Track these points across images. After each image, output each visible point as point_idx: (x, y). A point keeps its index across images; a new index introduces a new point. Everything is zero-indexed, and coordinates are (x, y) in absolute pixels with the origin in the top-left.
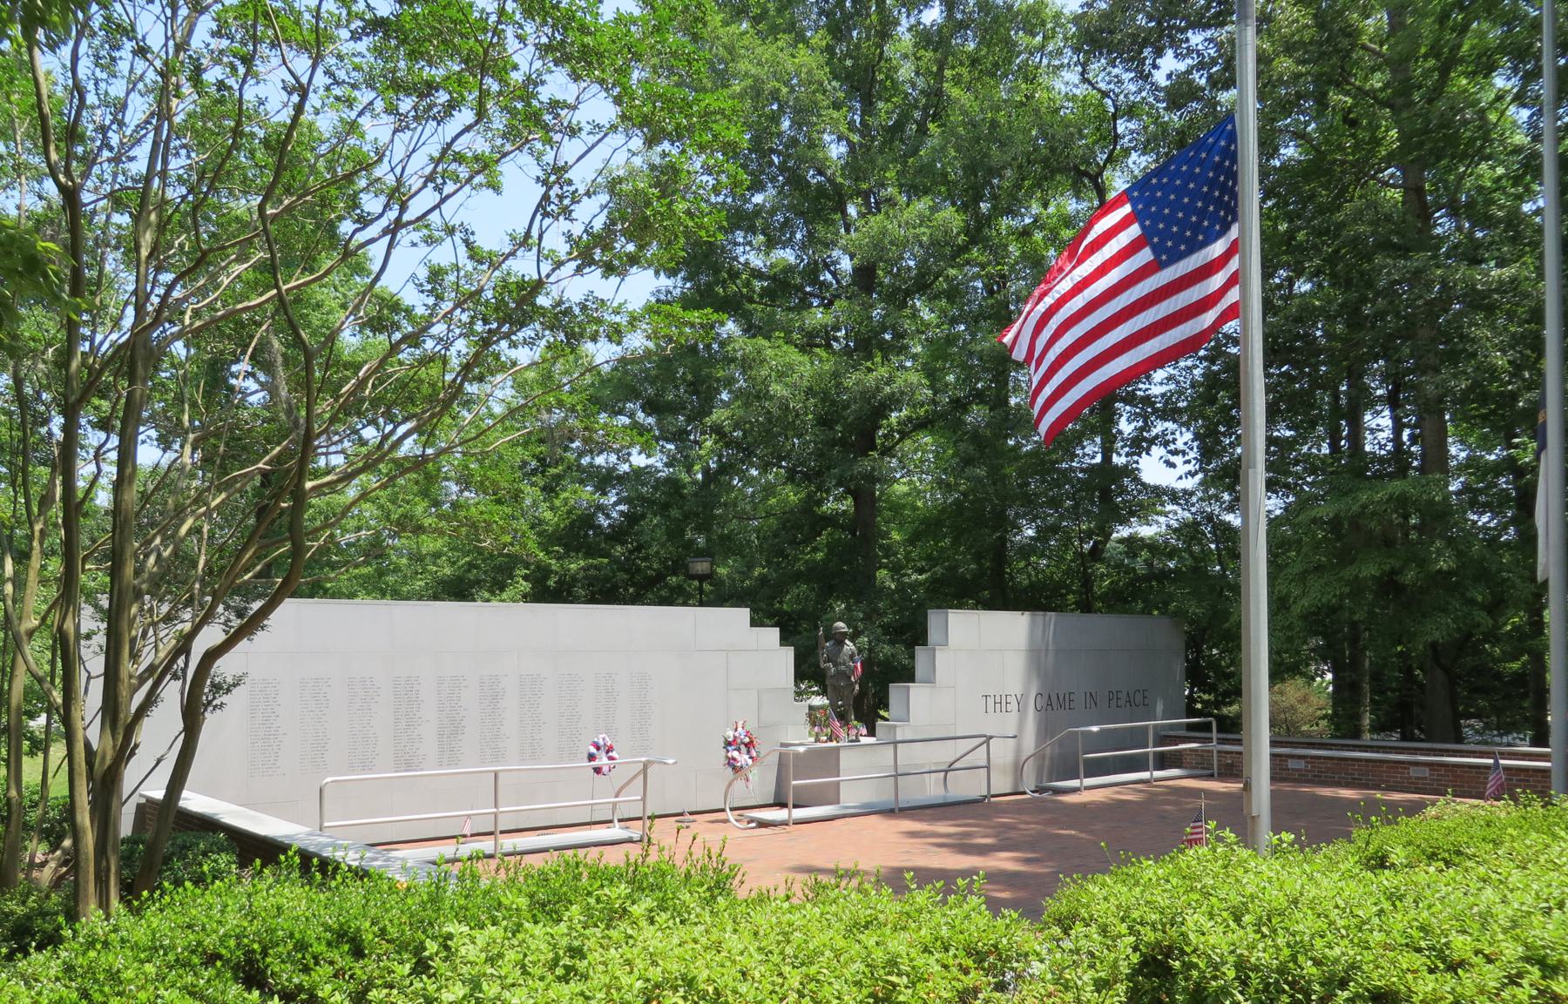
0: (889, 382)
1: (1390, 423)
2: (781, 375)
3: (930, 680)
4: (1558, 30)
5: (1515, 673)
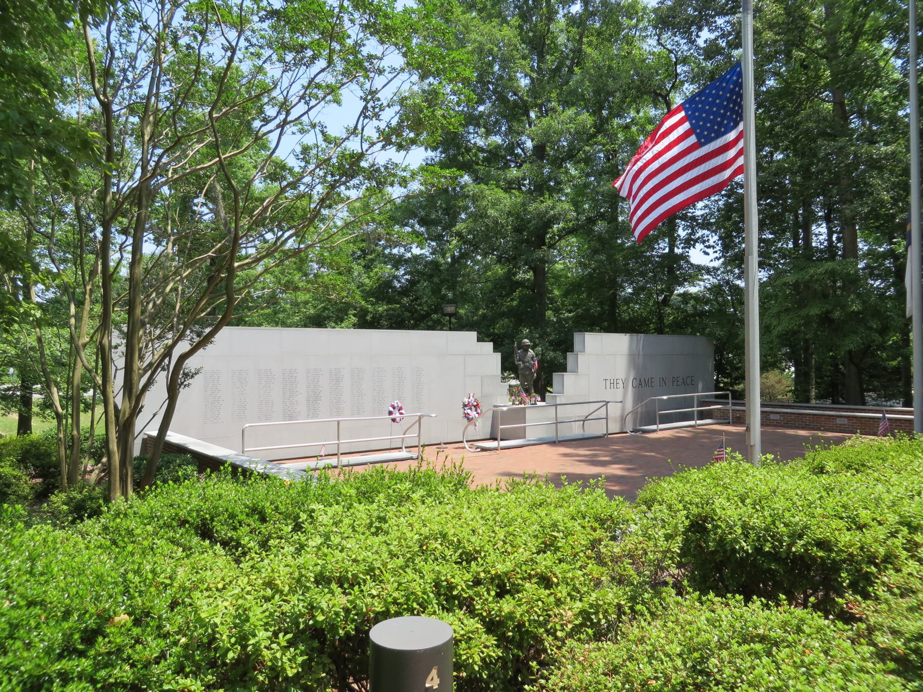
2: (494, 205)
3: (575, 371)
4: (918, 16)
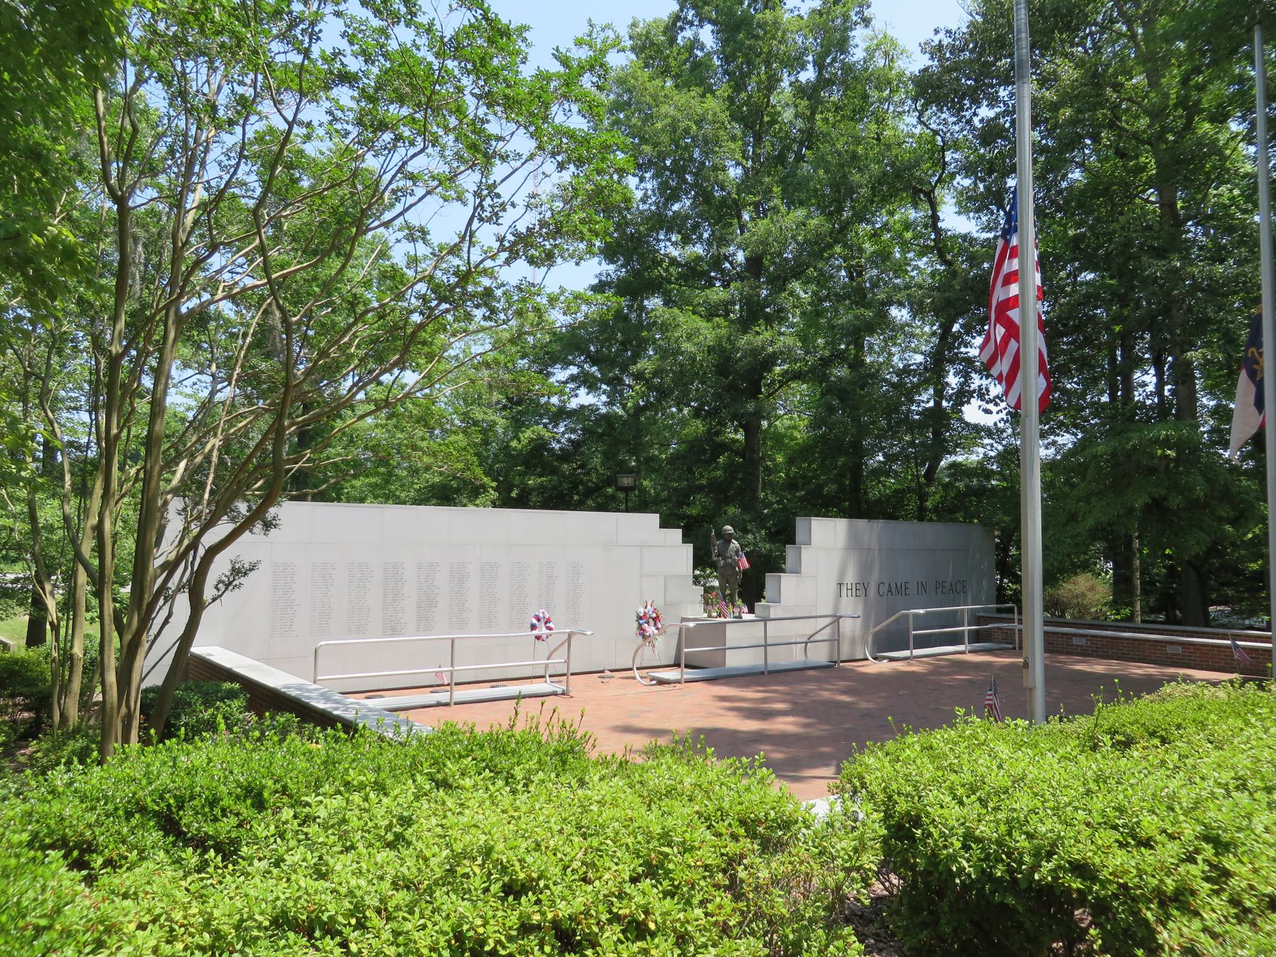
0: (772, 343)
1: (1154, 380)
2: (689, 338)
3: (797, 571)
4: (1267, 88)
5: (1254, 572)
